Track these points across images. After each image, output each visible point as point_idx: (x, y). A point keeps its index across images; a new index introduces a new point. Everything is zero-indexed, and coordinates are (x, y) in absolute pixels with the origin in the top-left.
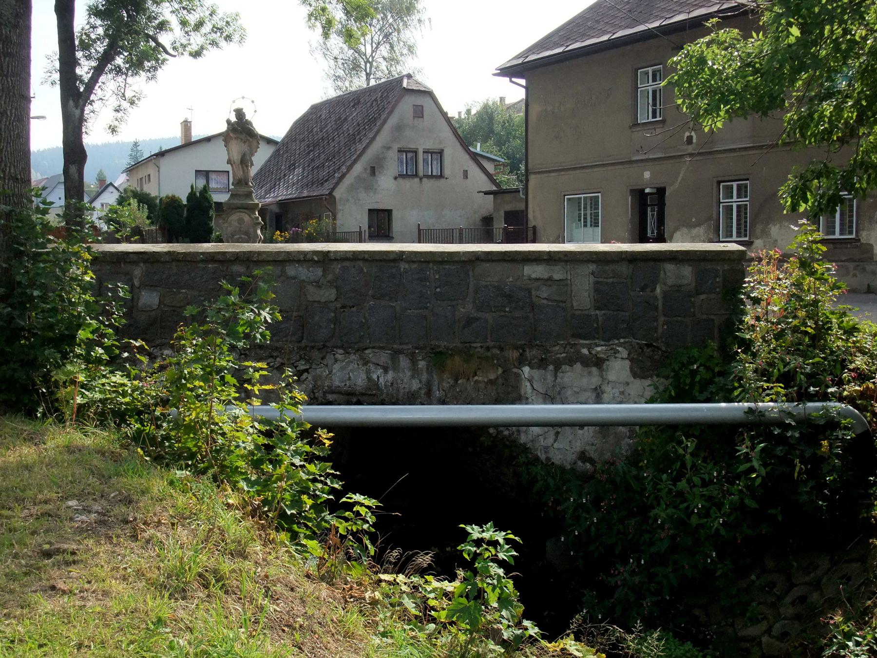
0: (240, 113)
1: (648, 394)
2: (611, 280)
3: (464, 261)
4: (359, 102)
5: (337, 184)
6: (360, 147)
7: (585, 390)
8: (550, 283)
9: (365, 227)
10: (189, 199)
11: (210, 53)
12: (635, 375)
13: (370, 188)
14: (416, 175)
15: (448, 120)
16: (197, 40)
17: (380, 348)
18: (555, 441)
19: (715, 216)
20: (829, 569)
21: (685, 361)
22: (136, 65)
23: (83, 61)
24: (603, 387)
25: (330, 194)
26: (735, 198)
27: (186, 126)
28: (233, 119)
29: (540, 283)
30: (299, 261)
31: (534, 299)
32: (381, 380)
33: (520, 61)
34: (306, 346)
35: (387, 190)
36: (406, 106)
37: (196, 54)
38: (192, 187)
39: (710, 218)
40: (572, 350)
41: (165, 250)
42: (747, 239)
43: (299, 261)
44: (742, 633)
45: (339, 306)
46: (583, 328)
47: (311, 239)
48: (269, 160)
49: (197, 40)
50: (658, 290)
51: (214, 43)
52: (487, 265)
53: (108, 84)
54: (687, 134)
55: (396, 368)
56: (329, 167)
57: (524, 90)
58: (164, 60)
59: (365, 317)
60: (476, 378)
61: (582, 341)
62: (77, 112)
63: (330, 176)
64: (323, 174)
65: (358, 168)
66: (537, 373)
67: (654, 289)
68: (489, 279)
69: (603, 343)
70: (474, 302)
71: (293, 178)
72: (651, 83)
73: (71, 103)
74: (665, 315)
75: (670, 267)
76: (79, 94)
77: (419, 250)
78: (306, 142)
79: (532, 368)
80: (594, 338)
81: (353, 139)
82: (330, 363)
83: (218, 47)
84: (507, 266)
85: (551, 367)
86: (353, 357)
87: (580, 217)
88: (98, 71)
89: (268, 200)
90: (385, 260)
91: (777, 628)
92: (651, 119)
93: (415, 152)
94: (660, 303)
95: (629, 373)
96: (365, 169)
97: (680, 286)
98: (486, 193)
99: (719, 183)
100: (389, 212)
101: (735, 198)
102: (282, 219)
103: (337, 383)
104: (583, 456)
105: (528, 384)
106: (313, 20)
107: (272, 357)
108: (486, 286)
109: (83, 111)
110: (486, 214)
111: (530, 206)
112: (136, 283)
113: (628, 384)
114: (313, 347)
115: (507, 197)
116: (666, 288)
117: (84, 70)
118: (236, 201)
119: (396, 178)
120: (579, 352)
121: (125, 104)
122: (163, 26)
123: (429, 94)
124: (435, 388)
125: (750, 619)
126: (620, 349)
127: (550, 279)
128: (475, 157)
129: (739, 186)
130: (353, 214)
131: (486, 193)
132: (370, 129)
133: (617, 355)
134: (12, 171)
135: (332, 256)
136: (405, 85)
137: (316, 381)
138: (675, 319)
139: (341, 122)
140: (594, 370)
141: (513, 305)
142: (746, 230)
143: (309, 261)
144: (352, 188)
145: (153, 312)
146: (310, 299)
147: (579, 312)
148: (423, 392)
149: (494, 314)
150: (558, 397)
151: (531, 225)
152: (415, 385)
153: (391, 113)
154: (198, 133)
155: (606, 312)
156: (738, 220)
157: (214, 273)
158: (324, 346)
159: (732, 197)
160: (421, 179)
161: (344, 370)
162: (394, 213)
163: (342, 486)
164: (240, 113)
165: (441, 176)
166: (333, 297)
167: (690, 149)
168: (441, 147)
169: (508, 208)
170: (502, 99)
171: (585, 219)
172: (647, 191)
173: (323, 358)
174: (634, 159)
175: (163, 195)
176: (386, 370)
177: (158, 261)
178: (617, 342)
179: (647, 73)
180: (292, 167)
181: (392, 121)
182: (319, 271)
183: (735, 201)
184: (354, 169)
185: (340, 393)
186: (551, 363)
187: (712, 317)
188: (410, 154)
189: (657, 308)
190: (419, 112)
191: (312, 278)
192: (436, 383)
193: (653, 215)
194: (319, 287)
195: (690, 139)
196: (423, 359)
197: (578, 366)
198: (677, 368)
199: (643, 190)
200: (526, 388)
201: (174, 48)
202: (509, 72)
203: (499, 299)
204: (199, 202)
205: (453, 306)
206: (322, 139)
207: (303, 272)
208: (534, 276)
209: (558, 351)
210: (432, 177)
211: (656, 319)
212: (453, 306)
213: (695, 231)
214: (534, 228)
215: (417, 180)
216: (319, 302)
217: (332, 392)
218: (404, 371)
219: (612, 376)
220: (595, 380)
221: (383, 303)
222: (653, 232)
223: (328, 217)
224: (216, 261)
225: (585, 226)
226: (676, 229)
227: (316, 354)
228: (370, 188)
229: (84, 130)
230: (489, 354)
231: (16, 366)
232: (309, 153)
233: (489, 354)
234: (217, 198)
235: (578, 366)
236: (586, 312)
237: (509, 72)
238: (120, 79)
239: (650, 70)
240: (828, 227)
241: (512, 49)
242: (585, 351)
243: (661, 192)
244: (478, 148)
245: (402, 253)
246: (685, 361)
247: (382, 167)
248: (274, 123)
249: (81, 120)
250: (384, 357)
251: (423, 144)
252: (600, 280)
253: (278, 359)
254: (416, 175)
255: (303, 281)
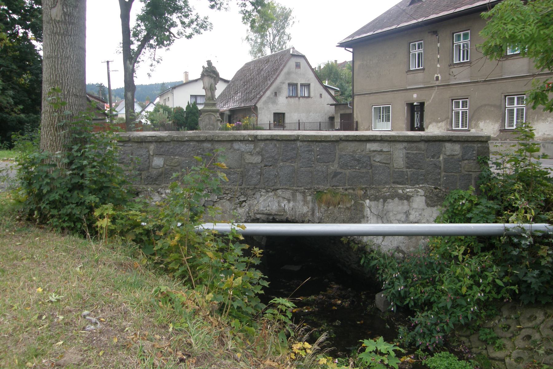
0: (209, 63)
1: (435, 215)
2: (415, 152)
3: (333, 141)
4: (269, 61)
5: (258, 100)
6: (269, 83)
7: (400, 213)
8: (381, 153)
9: (272, 122)
10: (187, 108)
11: (196, 36)
12: (428, 205)
13: (274, 103)
14: (297, 96)
15: (312, 69)
16: (189, 31)
17: (285, 189)
18: (383, 241)
19: (450, 116)
20: (544, 320)
21: (457, 198)
22: (160, 43)
23: (135, 42)
24: (410, 211)
25: (255, 106)
26: (461, 108)
27: (186, 74)
28: (206, 66)
29: (376, 153)
30: (241, 141)
31: (372, 162)
32: (286, 207)
33: (350, 39)
34: (245, 188)
35: (283, 103)
36: (292, 62)
37: (189, 37)
38: (188, 103)
39: (448, 118)
40: (393, 191)
41: (167, 135)
42: (467, 128)
43: (241, 141)
44: (493, 355)
45: (263, 165)
46: (401, 179)
47: (246, 128)
48: (225, 90)
49: (189, 31)
50: (441, 158)
51: (198, 32)
52: (346, 143)
53: (147, 53)
54: (436, 75)
55: (295, 200)
56: (254, 92)
57: (352, 54)
58: (173, 40)
59: (277, 172)
60: (339, 206)
61: (398, 186)
62: (131, 66)
63: (255, 97)
64: (252, 96)
65: (268, 93)
66: (373, 203)
67: (439, 157)
68: (347, 151)
69: (410, 187)
70: (339, 163)
71: (237, 98)
72: (417, 50)
73: (128, 62)
74: (445, 172)
75: (448, 145)
76: (132, 58)
77: (308, 134)
78: (243, 81)
79: (370, 200)
80: (405, 184)
81: (266, 79)
82: (258, 197)
83: (199, 33)
84: (356, 144)
85: (381, 200)
86: (270, 194)
87: (380, 117)
88: (141, 47)
89: (225, 109)
90: (289, 140)
91: (515, 354)
92: (417, 68)
93: (296, 85)
94: (442, 166)
95: (424, 203)
96: (272, 93)
97: (454, 155)
98: (331, 105)
99: (452, 100)
100: (284, 114)
101: (461, 108)
102: (232, 116)
103: (262, 209)
104: (398, 249)
105: (368, 209)
106: (245, 21)
107: (226, 193)
108: (345, 155)
109: (134, 66)
110: (331, 115)
111: (355, 111)
112: (151, 153)
113: (423, 209)
114: (248, 188)
115: (342, 107)
116: (445, 157)
117: (134, 47)
118: (207, 108)
119: (287, 98)
120: (396, 192)
121: (155, 63)
122: (173, 25)
123: (303, 57)
124: (316, 211)
125: (498, 347)
126: (419, 190)
127: (381, 151)
128: (326, 88)
129: (463, 102)
130: (265, 116)
131: (331, 105)
132: (274, 74)
133: (418, 194)
134: (74, 90)
135: (259, 138)
136: (291, 52)
137: (250, 207)
138: (451, 174)
139: (260, 71)
140: (405, 201)
141: (360, 165)
142: (466, 124)
143: (246, 140)
144: (266, 103)
145: (160, 170)
146: (247, 162)
147: (397, 170)
148: (310, 213)
149: (349, 171)
150: (385, 217)
151: (355, 120)
152: (305, 209)
153: (284, 66)
154: (191, 78)
155: (413, 169)
156: (462, 119)
157: (194, 147)
158: (255, 188)
159: (459, 107)
160: (299, 98)
161: (266, 202)
162: (287, 116)
163: (269, 285)
164: (209, 63)
165: (309, 97)
166: (260, 161)
167: (438, 83)
168: (309, 83)
169: (342, 112)
170: (336, 61)
171: (383, 117)
172: (415, 104)
173: (254, 194)
174: (408, 88)
175: (175, 107)
176: (289, 201)
177: (163, 141)
178: (418, 186)
179: (415, 45)
180: (236, 93)
181: (285, 70)
182: (252, 146)
183: (461, 109)
184: (267, 93)
185: (263, 214)
186: (381, 198)
187: (471, 173)
188: (293, 86)
189: (440, 168)
190: (298, 66)
191: (248, 150)
192: (317, 208)
193: (417, 116)
194: (252, 155)
195: (437, 78)
196: (310, 195)
197: (396, 199)
198: (452, 202)
199: (413, 103)
200: (367, 212)
201: (178, 35)
202: (344, 45)
203: (353, 162)
204: (192, 111)
205: (327, 166)
206: (251, 79)
207: (243, 147)
208: (372, 149)
209: (385, 190)
210: (305, 97)
211: (440, 174)
212: (327, 166)
213: (440, 124)
214: (357, 122)
215: (297, 99)
216: (252, 163)
217: (259, 214)
218: (299, 202)
219: (415, 205)
220: (406, 208)
221: (288, 164)
222: (417, 125)
223: (254, 116)
224: (195, 141)
225: (383, 121)
226: (430, 123)
227: (250, 192)
228: (274, 103)
229: (134, 75)
230: (347, 192)
231: (73, 206)
232: (244, 86)
233: (347, 192)
234: (200, 107)
235: (396, 199)
236: (401, 170)
237: (344, 45)
238: (152, 50)
239: (417, 43)
240: (510, 123)
241: (345, 34)
242: (400, 191)
243: (422, 104)
244: (326, 83)
245: (298, 136)
246: (457, 198)
247: (280, 92)
248: (228, 71)
249: (133, 71)
250: (288, 194)
251: (300, 81)
252: (409, 151)
253: (229, 195)
254: (297, 96)
255: (243, 151)
